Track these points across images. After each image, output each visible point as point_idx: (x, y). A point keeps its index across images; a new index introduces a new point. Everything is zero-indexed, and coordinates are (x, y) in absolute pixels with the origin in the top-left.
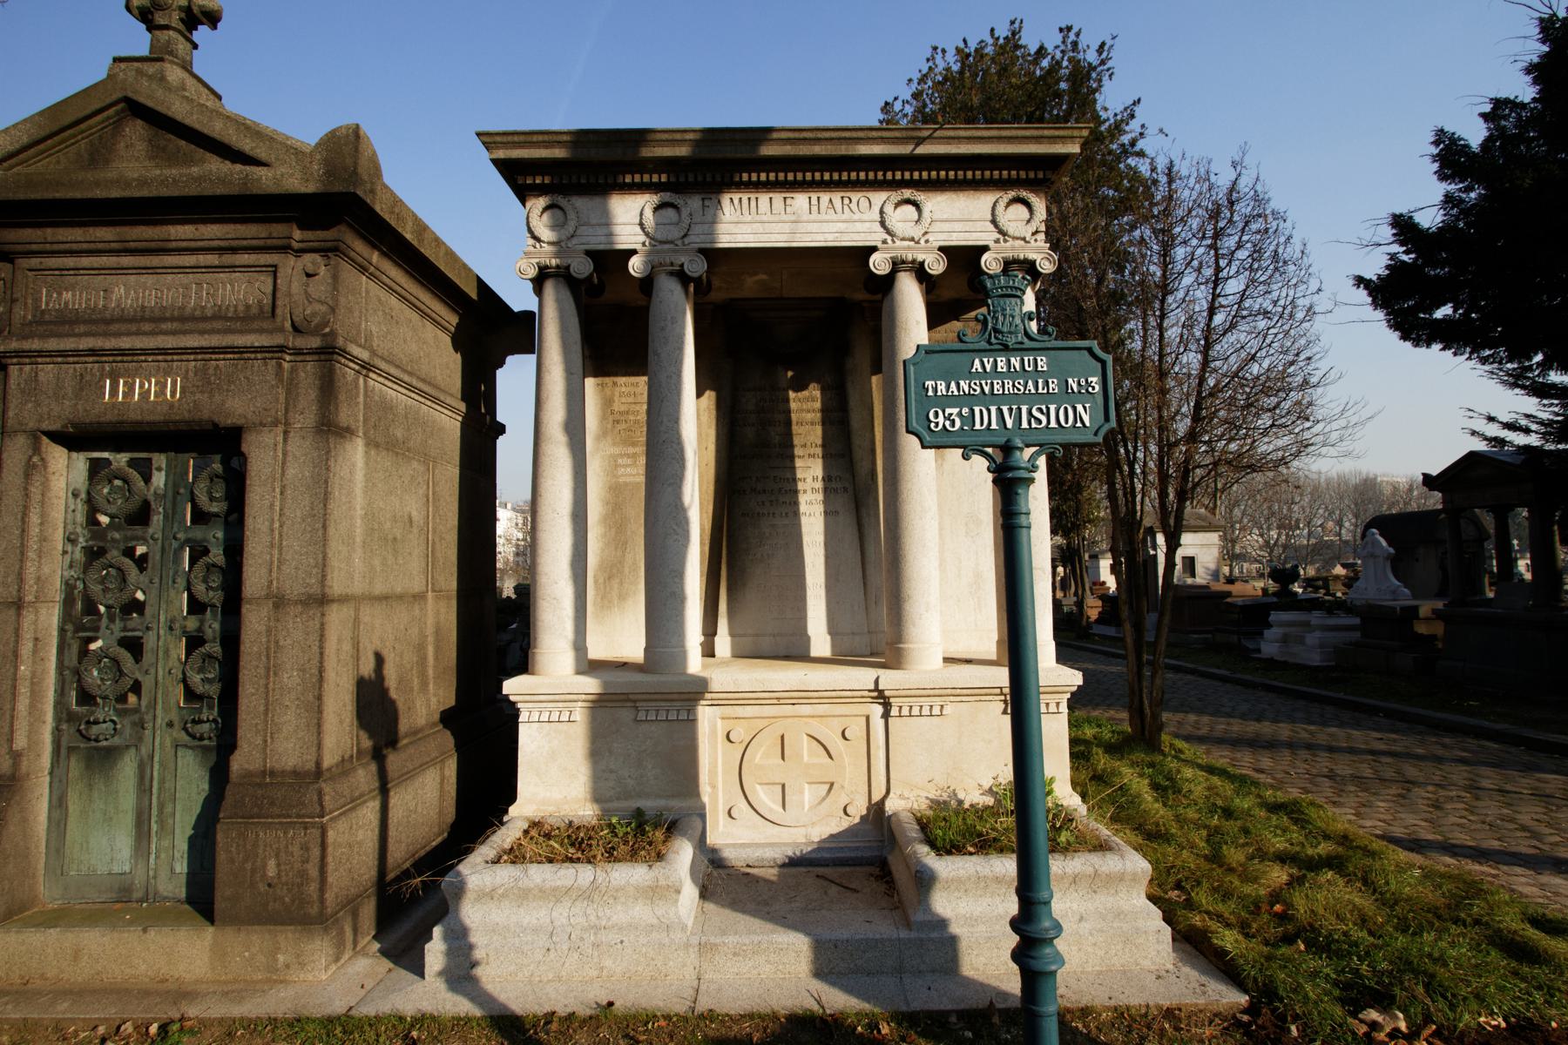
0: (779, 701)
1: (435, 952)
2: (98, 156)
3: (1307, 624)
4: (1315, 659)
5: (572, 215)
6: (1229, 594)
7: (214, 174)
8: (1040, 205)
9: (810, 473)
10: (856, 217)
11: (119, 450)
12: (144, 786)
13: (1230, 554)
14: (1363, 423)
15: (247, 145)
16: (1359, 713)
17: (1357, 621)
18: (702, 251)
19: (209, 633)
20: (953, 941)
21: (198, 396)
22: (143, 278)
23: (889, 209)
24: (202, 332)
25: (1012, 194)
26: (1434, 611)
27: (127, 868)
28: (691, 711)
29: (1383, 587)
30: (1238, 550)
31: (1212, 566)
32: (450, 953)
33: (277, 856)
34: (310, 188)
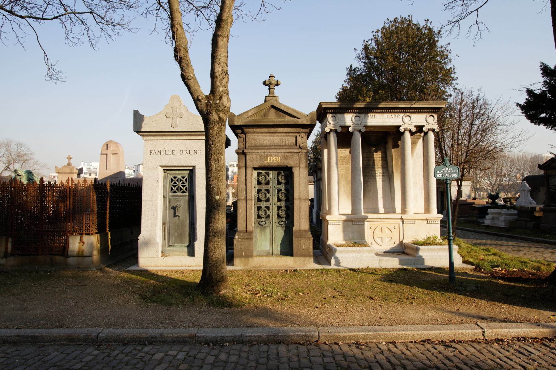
0: (381, 221)
1: (333, 261)
3: (500, 214)
4: (502, 225)
6: (474, 203)
7: (288, 120)
8: (436, 116)
9: (379, 172)
11: (263, 170)
13: (475, 189)
14: (527, 139)
15: (296, 115)
16: (513, 238)
17: (516, 212)
18: (364, 126)
19: (282, 206)
20: (423, 259)
23: (404, 117)
24: (285, 149)
25: (430, 114)
26: (540, 208)
28: (363, 222)
29: (526, 201)
30: (478, 187)
31: (468, 193)
32: (336, 261)
34: (308, 123)
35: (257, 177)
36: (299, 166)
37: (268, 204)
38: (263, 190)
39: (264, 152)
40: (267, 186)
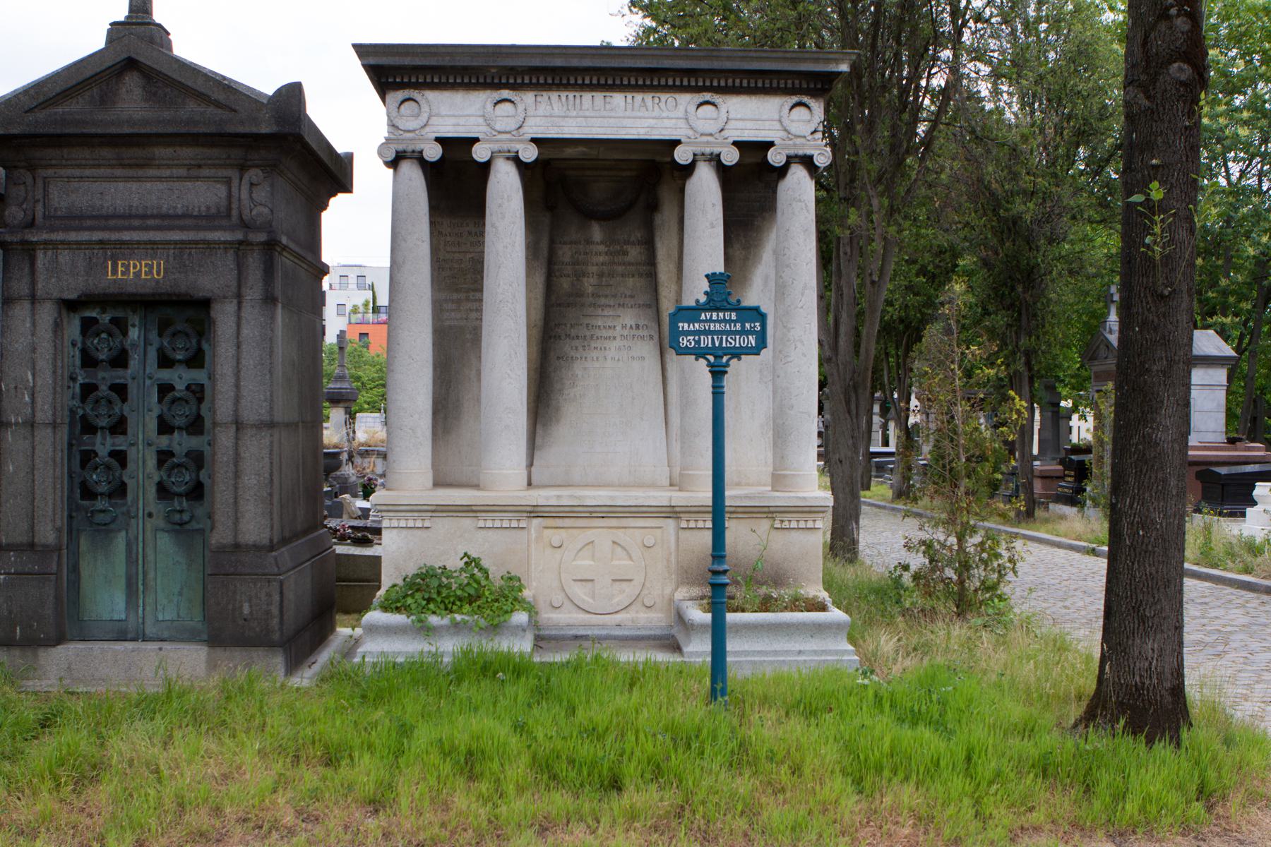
2: (106, 100)
5: (425, 108)
10: (664, 115)
12: (131, 559)
21: (177, 275)
22: (129, 185)
24: (182, 229)
25: (795, 99)
27: (123, 617)
33: (250, 601)
35: (79, 339)
36: (239, 297)
37: (120, 443)
38: (104, 389)
39: (101, 242)
40: (120, 372)
